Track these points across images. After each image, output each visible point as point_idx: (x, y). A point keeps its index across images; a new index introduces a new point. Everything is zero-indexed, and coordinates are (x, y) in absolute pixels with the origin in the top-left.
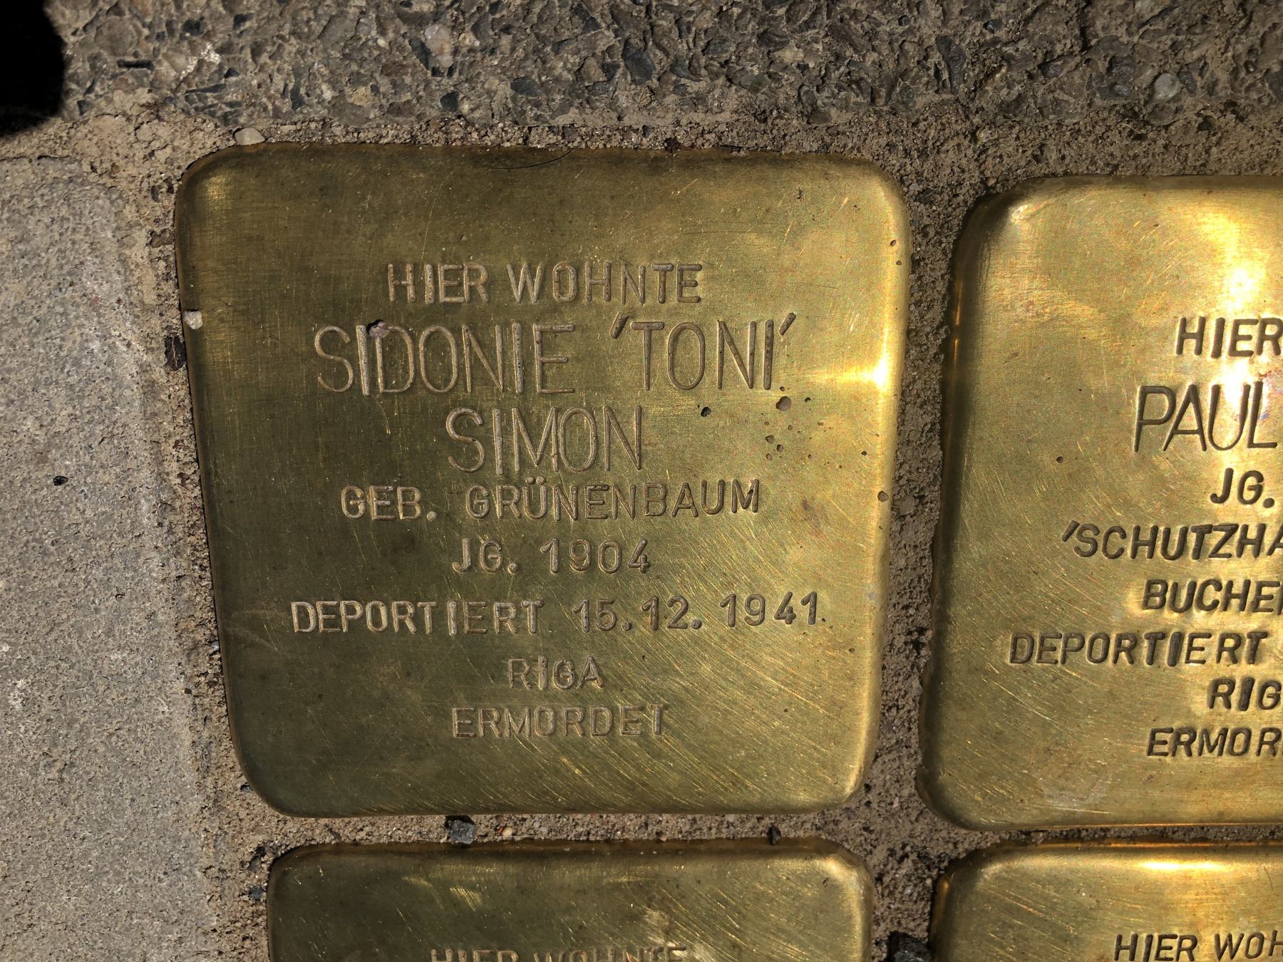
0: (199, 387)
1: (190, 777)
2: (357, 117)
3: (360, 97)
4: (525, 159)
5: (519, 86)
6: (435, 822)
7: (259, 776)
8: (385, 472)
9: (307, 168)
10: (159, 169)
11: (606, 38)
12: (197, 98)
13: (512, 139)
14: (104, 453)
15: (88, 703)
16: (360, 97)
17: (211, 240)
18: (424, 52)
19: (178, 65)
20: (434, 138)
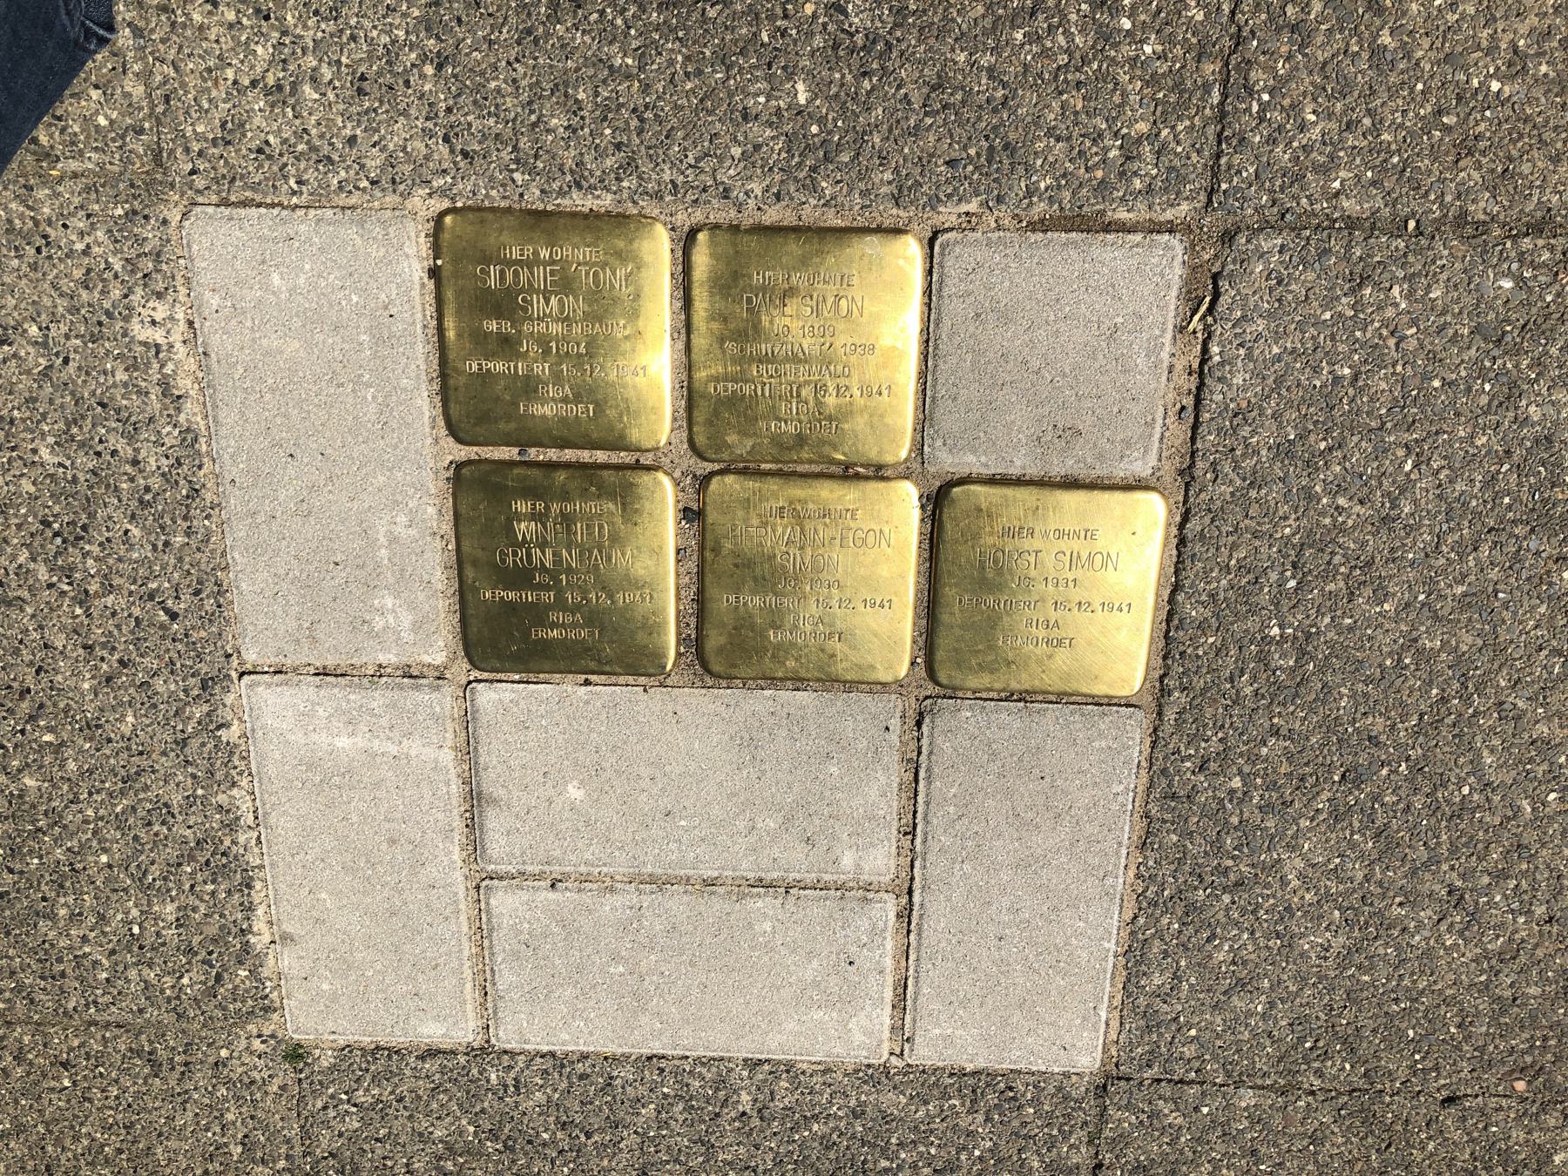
0: (438, 286)
1: (428, 430)
2: (493, 199)
3: (494, 193)
4: (545, 213)
5: (543, 191)
6: (515, 450)
7: (454, 431)
8: (499, 316)
9: (477, 212)
10: (430, 214)
11: (569, 178)
12: (443, 192)
13: (541, 207)
14: (406, 307)
15: (394, 398)
16: (494, 193)
17: (446, 236)
18: (513, 181)
19: (438, 182)
20: (517, 206)
